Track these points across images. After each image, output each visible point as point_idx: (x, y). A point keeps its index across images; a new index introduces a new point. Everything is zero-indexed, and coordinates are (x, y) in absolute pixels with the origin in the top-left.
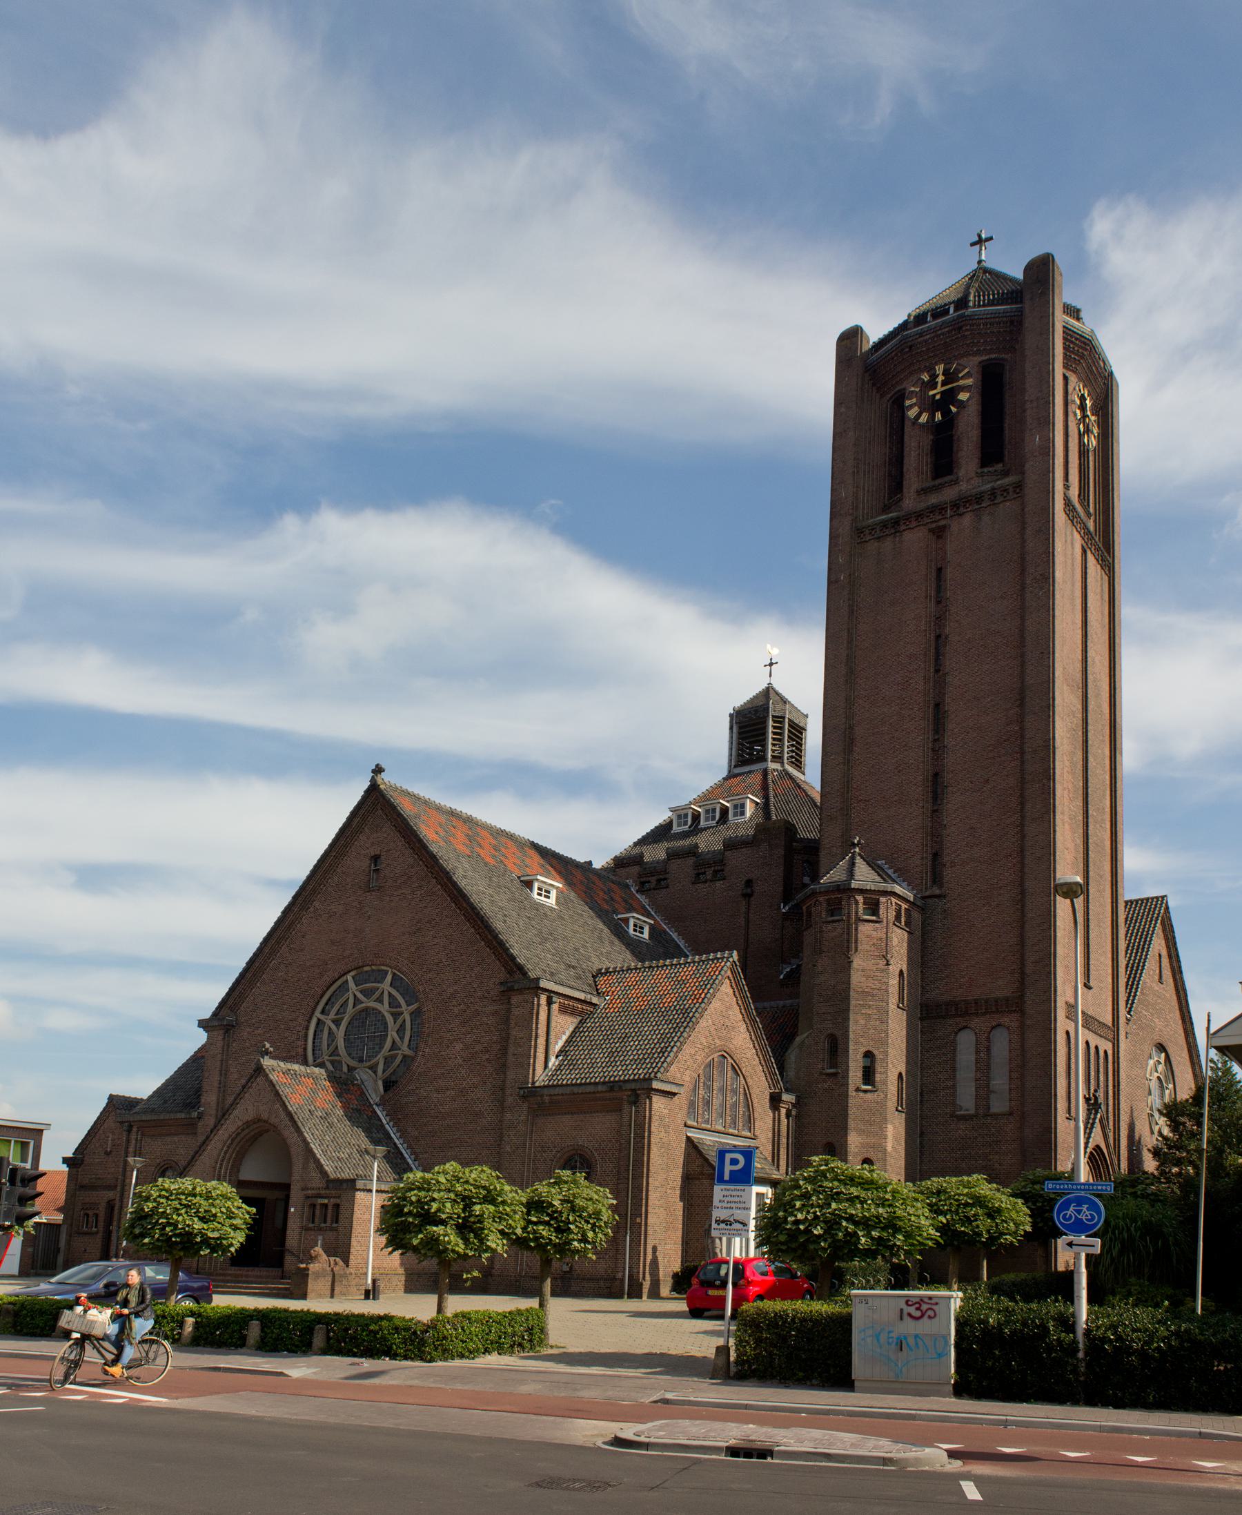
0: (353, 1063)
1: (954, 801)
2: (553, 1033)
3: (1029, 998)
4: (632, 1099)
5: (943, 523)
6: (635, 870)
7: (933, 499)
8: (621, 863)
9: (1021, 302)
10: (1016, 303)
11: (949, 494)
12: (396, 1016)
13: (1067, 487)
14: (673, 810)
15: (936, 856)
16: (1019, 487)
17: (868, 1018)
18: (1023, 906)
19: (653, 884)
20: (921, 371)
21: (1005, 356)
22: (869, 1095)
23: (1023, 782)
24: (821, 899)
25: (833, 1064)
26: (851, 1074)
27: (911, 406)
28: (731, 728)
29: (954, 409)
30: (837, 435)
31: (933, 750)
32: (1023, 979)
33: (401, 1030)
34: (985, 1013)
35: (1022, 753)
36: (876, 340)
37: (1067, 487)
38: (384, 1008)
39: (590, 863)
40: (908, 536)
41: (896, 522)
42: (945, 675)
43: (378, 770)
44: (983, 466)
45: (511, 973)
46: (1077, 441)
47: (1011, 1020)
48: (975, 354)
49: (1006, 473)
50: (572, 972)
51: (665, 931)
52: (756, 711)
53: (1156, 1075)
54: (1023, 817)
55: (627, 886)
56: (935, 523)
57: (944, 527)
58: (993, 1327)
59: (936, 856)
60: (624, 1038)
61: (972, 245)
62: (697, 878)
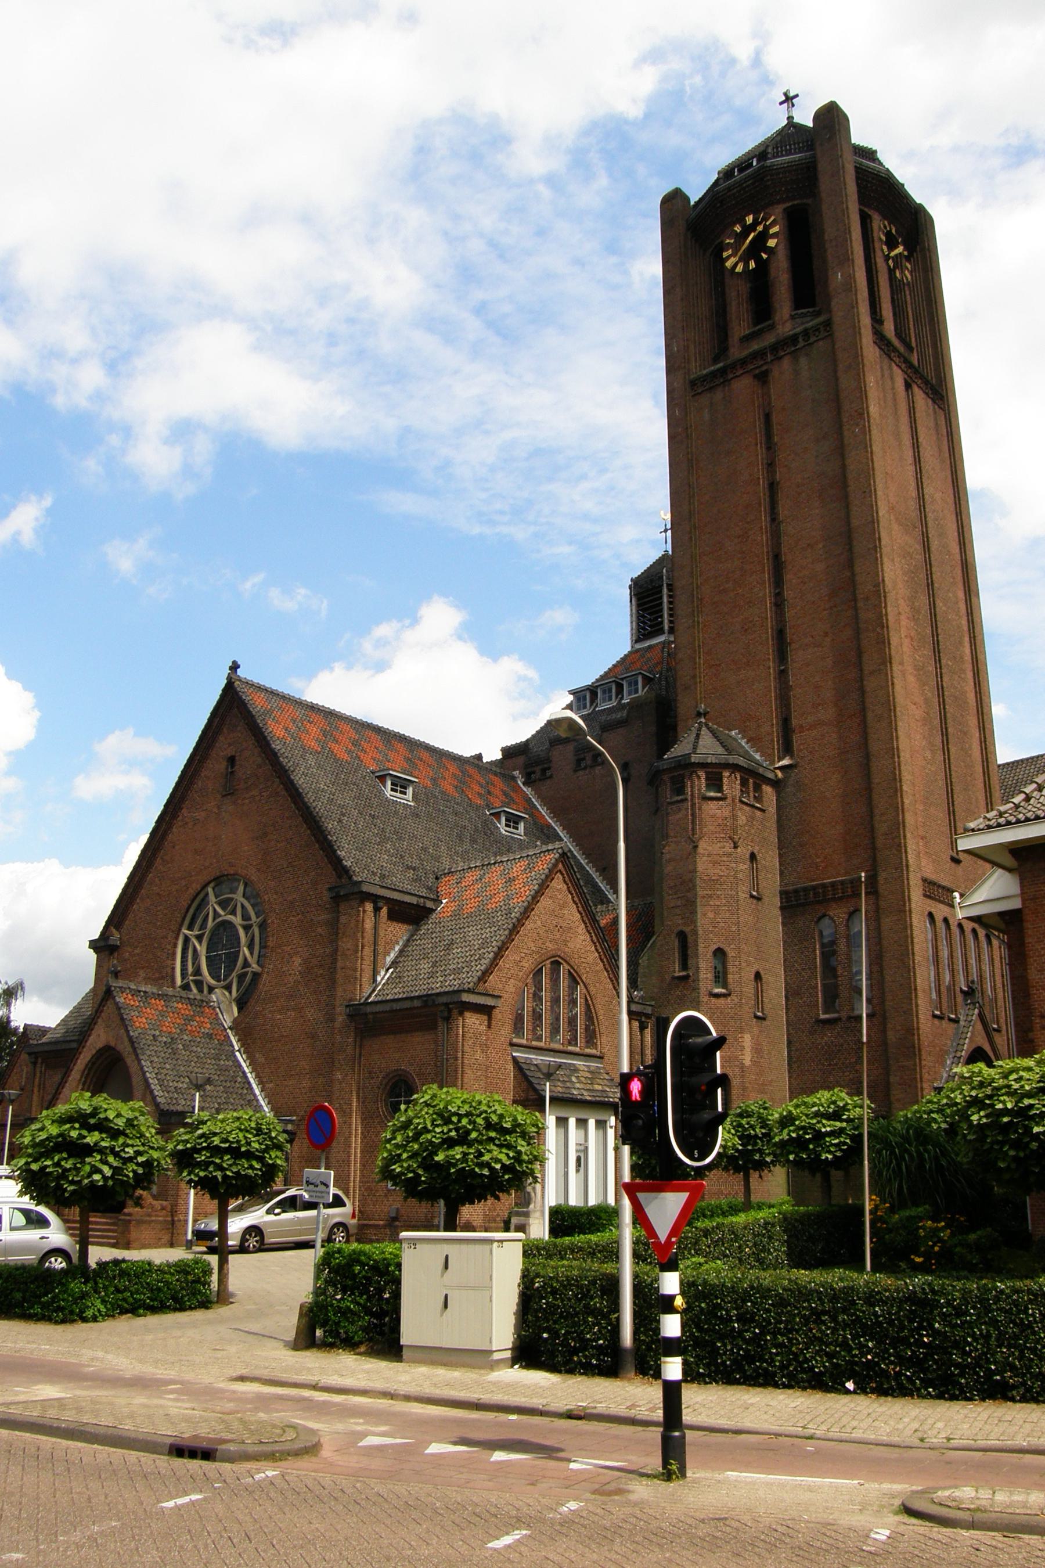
0: (213, 982)
1: (798, 657)
2: (381, 942)
4: (446, 1014)
5: (764, 368)
6: (521, 760)
7: (755, 346)
8: (509, 753)
11: (770, 339)
12: (247, 928)
16: (828, 324)
17: (717, 909)
19: (538, 775)
20: (734, 224)
21: (809, 201)
22: (722, 1001)
23: (857, 632)
24: (666, 777)
25: (684, 966)
26: (702, 976)
27: (728, 258)
29: (765, 256)
33: (251, 947)
34: (841, 899)
35: (855, 600)
36: (697, 199)
38: (237, 920)
39: (479, 757)
41: (723, 371)
42: (779, 524)
43: (235, 667)
44: (797, 308)
45: (340, 877)
48: (779, 202)
49: (818, 314)
51: (549, 826)
52: (652, 581)
54: (861, 670)
55: (514, 778)
57: (767, 370)
58: (398, 1235)
60: (448, 948)
61: (781, 103)
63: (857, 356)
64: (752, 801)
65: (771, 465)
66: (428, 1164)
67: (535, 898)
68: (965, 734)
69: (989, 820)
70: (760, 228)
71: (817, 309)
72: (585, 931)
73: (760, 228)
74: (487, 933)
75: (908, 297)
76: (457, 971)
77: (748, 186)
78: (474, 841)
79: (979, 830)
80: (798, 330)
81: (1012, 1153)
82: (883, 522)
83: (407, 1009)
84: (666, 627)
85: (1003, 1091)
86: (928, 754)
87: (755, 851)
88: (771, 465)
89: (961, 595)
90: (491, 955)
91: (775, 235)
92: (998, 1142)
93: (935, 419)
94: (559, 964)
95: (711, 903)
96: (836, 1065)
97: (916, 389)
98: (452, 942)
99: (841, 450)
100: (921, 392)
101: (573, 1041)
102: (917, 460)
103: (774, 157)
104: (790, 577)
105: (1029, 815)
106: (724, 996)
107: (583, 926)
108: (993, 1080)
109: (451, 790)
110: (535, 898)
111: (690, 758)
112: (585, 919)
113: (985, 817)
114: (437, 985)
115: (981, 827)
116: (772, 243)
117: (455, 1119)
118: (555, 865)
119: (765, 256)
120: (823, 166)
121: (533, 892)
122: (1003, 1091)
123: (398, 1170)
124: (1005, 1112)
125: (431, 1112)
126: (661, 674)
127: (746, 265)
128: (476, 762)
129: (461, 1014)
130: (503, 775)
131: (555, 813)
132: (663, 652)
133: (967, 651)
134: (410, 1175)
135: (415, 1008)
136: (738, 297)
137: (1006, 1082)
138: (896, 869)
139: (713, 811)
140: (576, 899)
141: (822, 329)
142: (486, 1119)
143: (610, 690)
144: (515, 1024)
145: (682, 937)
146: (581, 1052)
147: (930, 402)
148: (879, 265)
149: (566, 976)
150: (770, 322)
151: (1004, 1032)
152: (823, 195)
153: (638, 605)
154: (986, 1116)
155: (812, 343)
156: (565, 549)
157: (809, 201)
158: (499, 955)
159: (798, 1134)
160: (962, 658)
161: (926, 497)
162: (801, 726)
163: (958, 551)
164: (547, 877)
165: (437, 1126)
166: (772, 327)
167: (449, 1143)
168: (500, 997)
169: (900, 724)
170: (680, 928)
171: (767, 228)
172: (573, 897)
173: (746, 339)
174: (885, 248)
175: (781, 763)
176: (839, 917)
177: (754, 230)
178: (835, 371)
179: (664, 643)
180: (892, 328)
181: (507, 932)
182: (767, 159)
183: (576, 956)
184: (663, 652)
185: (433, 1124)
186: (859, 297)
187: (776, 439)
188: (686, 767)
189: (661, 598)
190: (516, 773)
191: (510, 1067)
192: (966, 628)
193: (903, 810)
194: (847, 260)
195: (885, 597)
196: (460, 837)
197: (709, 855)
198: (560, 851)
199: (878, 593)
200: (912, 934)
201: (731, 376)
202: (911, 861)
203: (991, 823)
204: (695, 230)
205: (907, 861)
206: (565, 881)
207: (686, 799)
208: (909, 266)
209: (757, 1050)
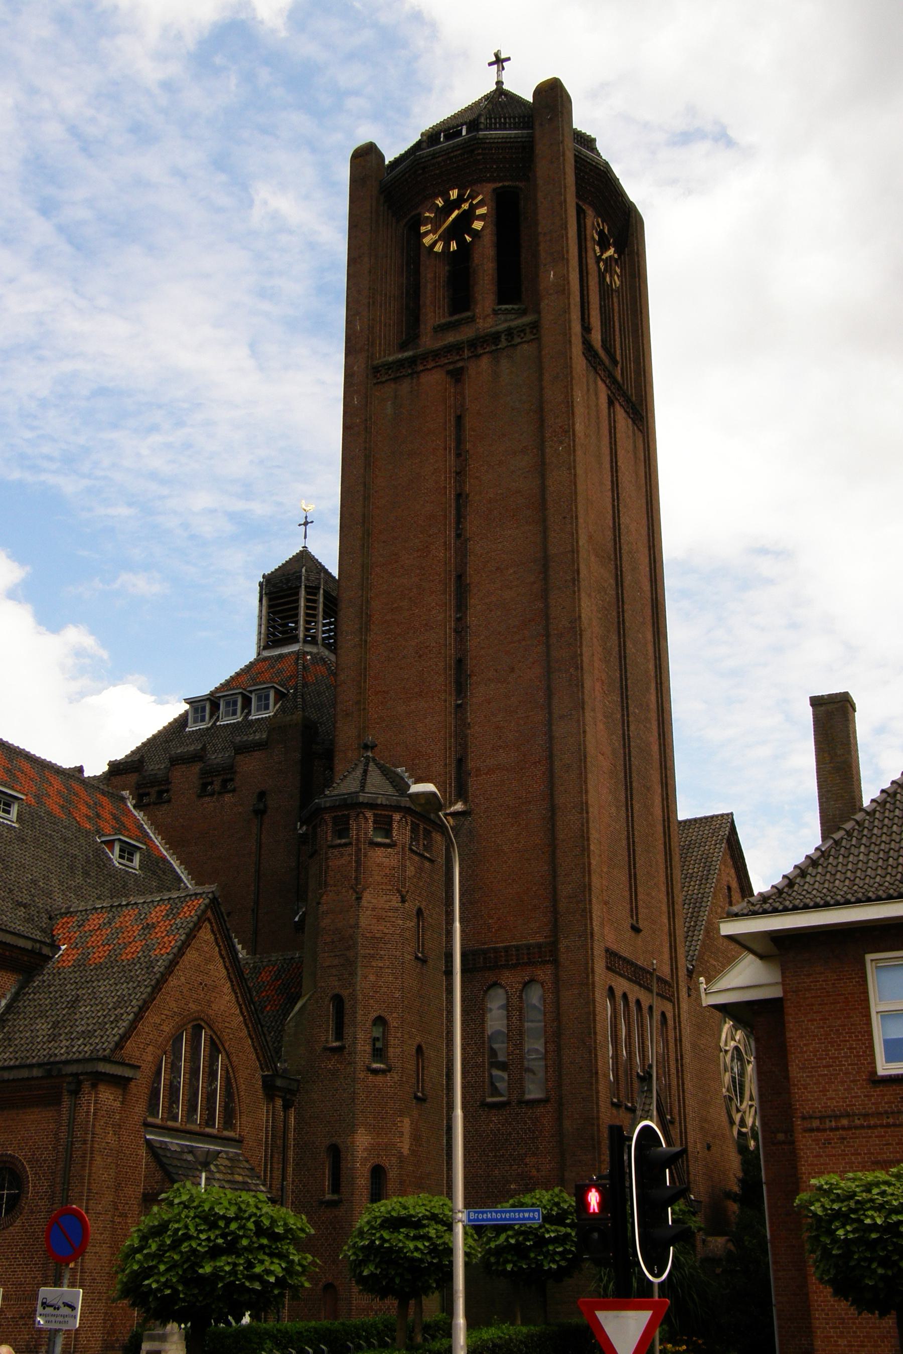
3: (563, 944)
4: (73, 1087)
5: (460, 364)
6: (133, 778)
7: (451, 338)
8: (116, 769)
9: (532, 128)
10: (528, 128)
11: (466, 333)
13: (586, 329)
14: (189, 701)
15: (461, 762)
16: (535, 326)
18: (553, 825)
19: (153, 798)
20: (436, 197)
21: (521, 185)
22: (380, 1078)
24: (327, 817)
25: (339, 1036)
26: (359, 1047)
27: (427, 233)
28: (261, 600)
29: (468, 239)
30: (352, 261)
31: (456, 631)
32: (556, 919)
34: (515, 966)
35: (548, 636)
36: (392, 159)
37: (586, 329)
39: (80, 769)
40: (425, 378)
41: (413, 361)
44: (500, 303)
46: (596, 280)
47: (544, 974)
48: (489, 181)
49: (524, 313)
50: (21, 912)
51: (164, 859)
53: (733, 1044)
54: (550, 713)
56: (455, 363)
57: (462, 368)
59: (461, 762)
60: (74, 1003)
62: (204, 790)
63: (568, 366)
64: (421, 850)
65: (460, 474)
66: (192, 1280)
67: (181, 951)
68: (648, 789)
69: (753, 905)
70: (465, 206)
71: (523, 307)
72: (230, 990)
73: (465, 206)
74: (124, 989)
75: (616, 305)
76: (87, 1034)
77: (455, 156)
78: (86, 874)
79: (743, 915)
80: (502, 327)
81: (880, 1271)
82: (583, 554)
83: (23, 1079)
84: (301, 636)
85: (868, 1205)
86: (613, 810)
87: (422, 907)
88: (460, 474)
89: (649, 636)
90: (131, 1016)
91: (481, 217)
92: (865, 1259)
93: (634, 442)
94: (201, 1028)
95: (374, 964)
96: (503, 1156)
97: (618, 408)
98: (77, 999)
99: (541, 468)
100: (623, 411)
101: (209, 1121)
102: (615, 484)
103: (486, 129)
104: (475, 602)
105: (797, 902)
106: (383, 1072)
107: (229, 984)
108: (855, 1194)
109: (57, 810)
110: (181, 951)
111: (357, 797)
112: (232, 976)
113: (749, 902)
114: (61, 1051)
115: (745, 911)
116: (478, 225)
117: (222, 1224)
118: (204, 912)
119: (468, 239)
120: (542, 148)
121: (179, 943)
122: (868, 1205)
123: (154, 1286)
124: (874, 1227)
125: (192, 1214)
126: (296, 690)
127: (447, 246)
128: (77, 774)
129: (94, 1086)
130: (111, 796)
131: (173, 844)
132: (297, 664)
133: (653, 698)
134: (168, 1292)
135: (33, 1078)
136: (433, 280)
137: (869, 1196)
138: (580, 937)
139: (381, 859)
140: (223, 952)
141: (528, 331)
142: (256, 1223)
143: (235, 703)
144: (150, 1099)
145: (338, 1000)
146: (220, 1134)
147: (630, 421)
148: (590, 266)
149: (208, 1043)
150: (469, 314)
151: (677, 1125)
152: (540, 182)
153: (270, 607)
154: (853, 1232)
155: (517, 345)
156: (123, 511)
157: (521, 185)
158: (139, 1016)
159: (517, 1240)
160: (648, 706)
161: (622, 526)
162: (478, 770)
163: (649, 588)
164: (195, 925)
165: (201, 1231)
166: (472, 320)
167: (215, 1252)
168: (139, 1067)
169: (589, 776)
170: (336, 991)
171: (473, 208)
172: (220, 951)
173: (441, 329)
174: (597, 248)
175: (452, 809)
176: (512, 987)
177: (459, 208)
178: (540, 379)
179: (297, 653)
180: (599, 338)
181: (149, 990)
182: (479, 130)
183: (220, 1020)
184: (297, 664)
185: (196, 1230)
186: (572, 301)
187: (468, 446)
188: (352, 806)
189: (297, 601)
190: (126, 793)
191: (143, 1152)
192: (652, 674)
193: (589, 871)
194: (562, 258)
195: (581, 635)
196: (71, 868)
197: (374, 909)
198: (210, 895)
199: (575, 629)
200: (594, 1011)
201: (421, 368)
202: (596, 928)
203: (756, 908)
204: (390, 196)
205: (592, 929)
206: (213, 931)
207: (351, 844)
208: (618, 270)
209: (416, 1138)
